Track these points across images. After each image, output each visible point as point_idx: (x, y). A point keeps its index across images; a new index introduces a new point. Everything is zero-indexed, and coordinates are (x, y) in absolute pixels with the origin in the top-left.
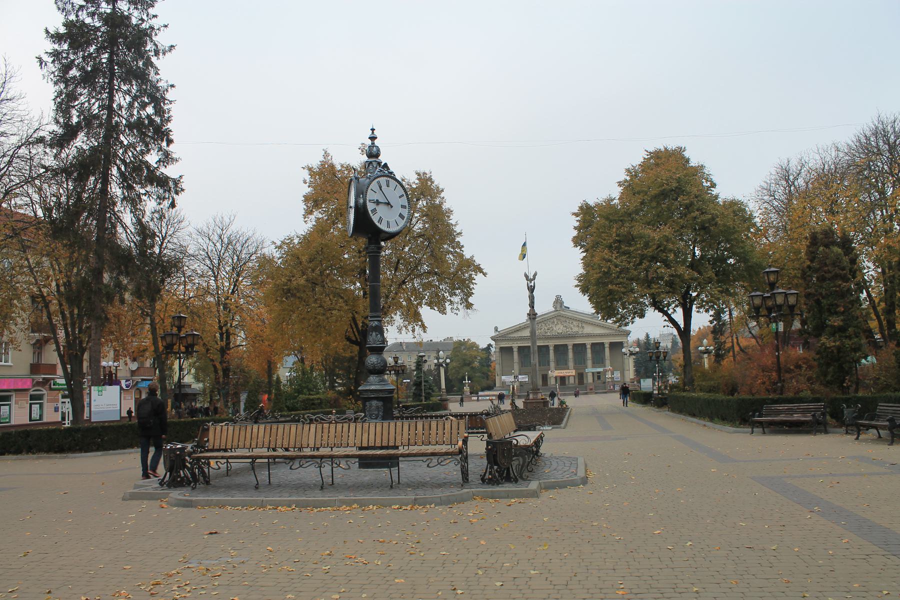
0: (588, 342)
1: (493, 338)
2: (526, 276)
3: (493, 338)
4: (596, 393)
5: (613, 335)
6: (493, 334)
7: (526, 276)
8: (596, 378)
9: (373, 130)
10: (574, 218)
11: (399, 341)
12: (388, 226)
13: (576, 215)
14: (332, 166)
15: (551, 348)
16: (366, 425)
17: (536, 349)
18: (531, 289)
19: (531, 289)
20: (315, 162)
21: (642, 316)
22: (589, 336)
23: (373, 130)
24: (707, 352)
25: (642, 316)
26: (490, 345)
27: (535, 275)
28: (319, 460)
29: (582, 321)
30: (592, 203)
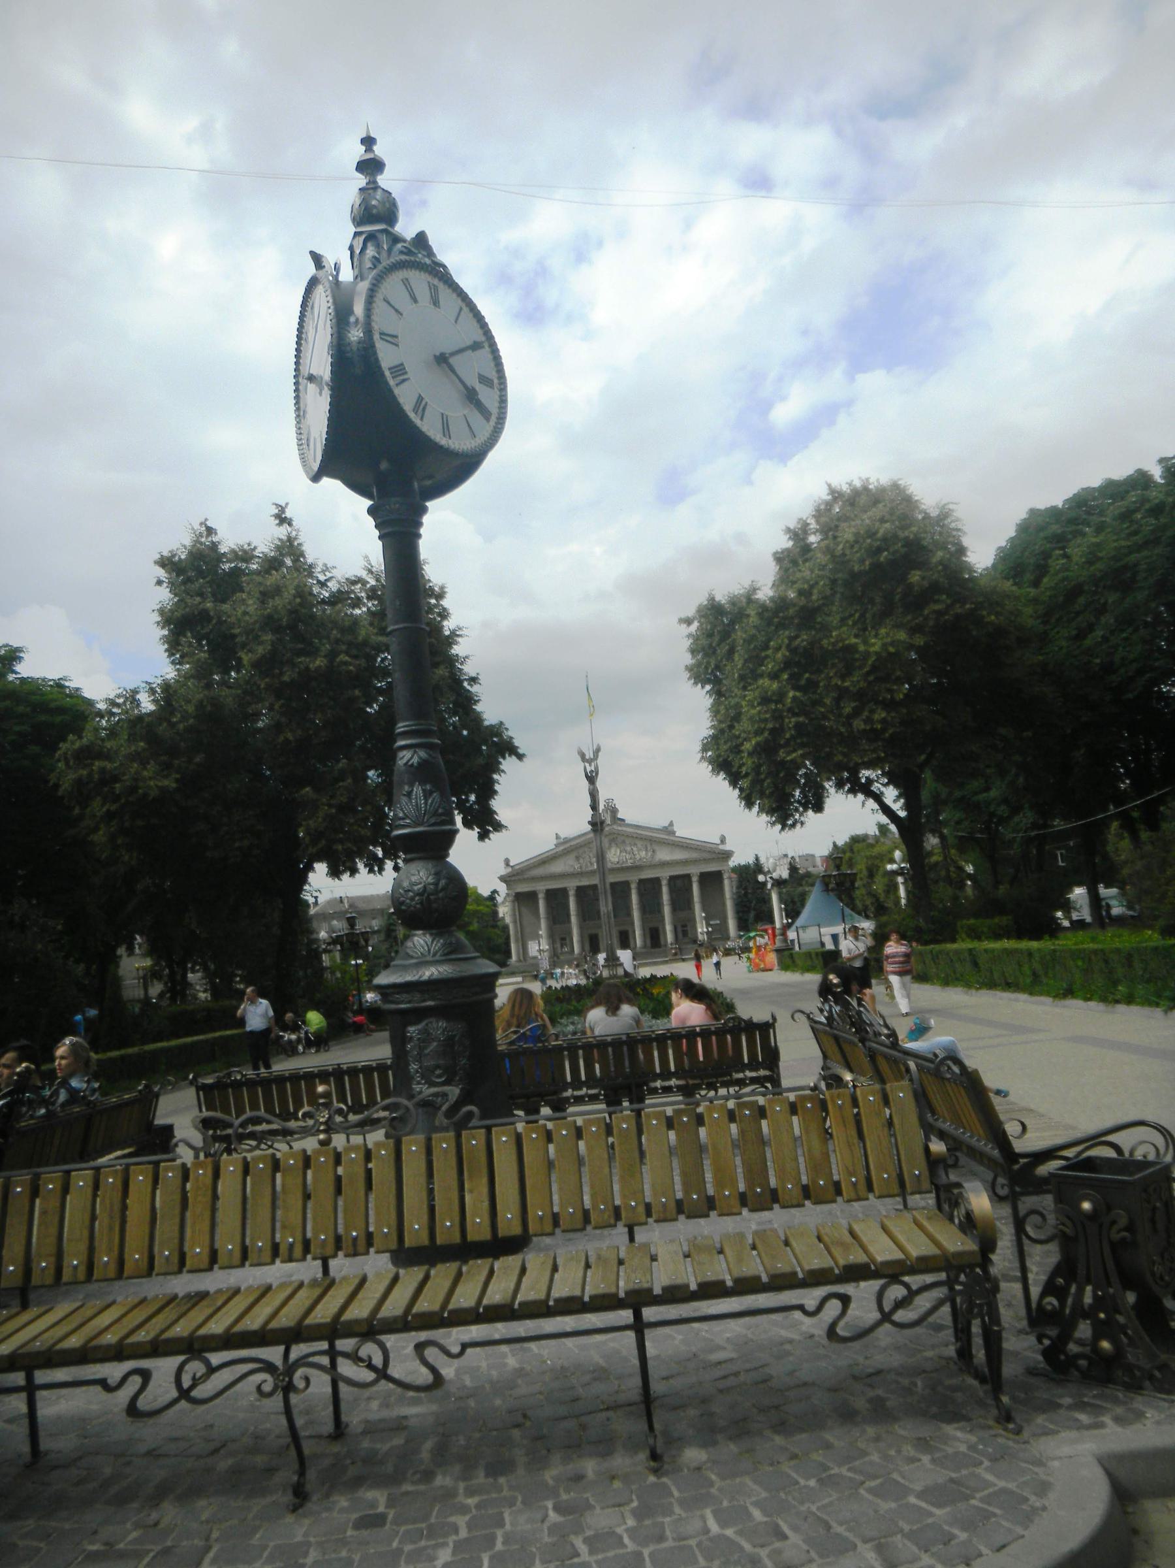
0: (664, 874)
1: (503, 879)
2: (583, 756)
3: (503, 879)
4: (684, 960)
5: (706, 860)
6: (503, 871)
7: (583, 756)
8: (680, 935)
9: (368, 142)
10: (685, 630)
11: (337, 895)
12: (446, 430)
13: (688, 622)
14: (214, 546)
15: (572, 893)
16: (474, 1140)
17: (608, 887)
18: (591, 778)
19: (591, 778)
20: (179, 542)
21: (819, 807)
22: (664, 864)
23: (368, 142)
24: (900, 872)
25: (819, 807)
26: (495, 892)
27: (597, 751)
28: (274, 1354)
29: (651, 841)
30: (721, 597)
